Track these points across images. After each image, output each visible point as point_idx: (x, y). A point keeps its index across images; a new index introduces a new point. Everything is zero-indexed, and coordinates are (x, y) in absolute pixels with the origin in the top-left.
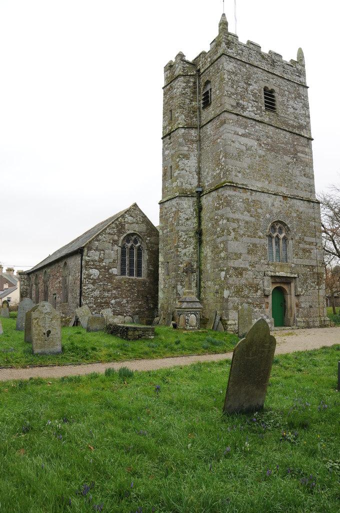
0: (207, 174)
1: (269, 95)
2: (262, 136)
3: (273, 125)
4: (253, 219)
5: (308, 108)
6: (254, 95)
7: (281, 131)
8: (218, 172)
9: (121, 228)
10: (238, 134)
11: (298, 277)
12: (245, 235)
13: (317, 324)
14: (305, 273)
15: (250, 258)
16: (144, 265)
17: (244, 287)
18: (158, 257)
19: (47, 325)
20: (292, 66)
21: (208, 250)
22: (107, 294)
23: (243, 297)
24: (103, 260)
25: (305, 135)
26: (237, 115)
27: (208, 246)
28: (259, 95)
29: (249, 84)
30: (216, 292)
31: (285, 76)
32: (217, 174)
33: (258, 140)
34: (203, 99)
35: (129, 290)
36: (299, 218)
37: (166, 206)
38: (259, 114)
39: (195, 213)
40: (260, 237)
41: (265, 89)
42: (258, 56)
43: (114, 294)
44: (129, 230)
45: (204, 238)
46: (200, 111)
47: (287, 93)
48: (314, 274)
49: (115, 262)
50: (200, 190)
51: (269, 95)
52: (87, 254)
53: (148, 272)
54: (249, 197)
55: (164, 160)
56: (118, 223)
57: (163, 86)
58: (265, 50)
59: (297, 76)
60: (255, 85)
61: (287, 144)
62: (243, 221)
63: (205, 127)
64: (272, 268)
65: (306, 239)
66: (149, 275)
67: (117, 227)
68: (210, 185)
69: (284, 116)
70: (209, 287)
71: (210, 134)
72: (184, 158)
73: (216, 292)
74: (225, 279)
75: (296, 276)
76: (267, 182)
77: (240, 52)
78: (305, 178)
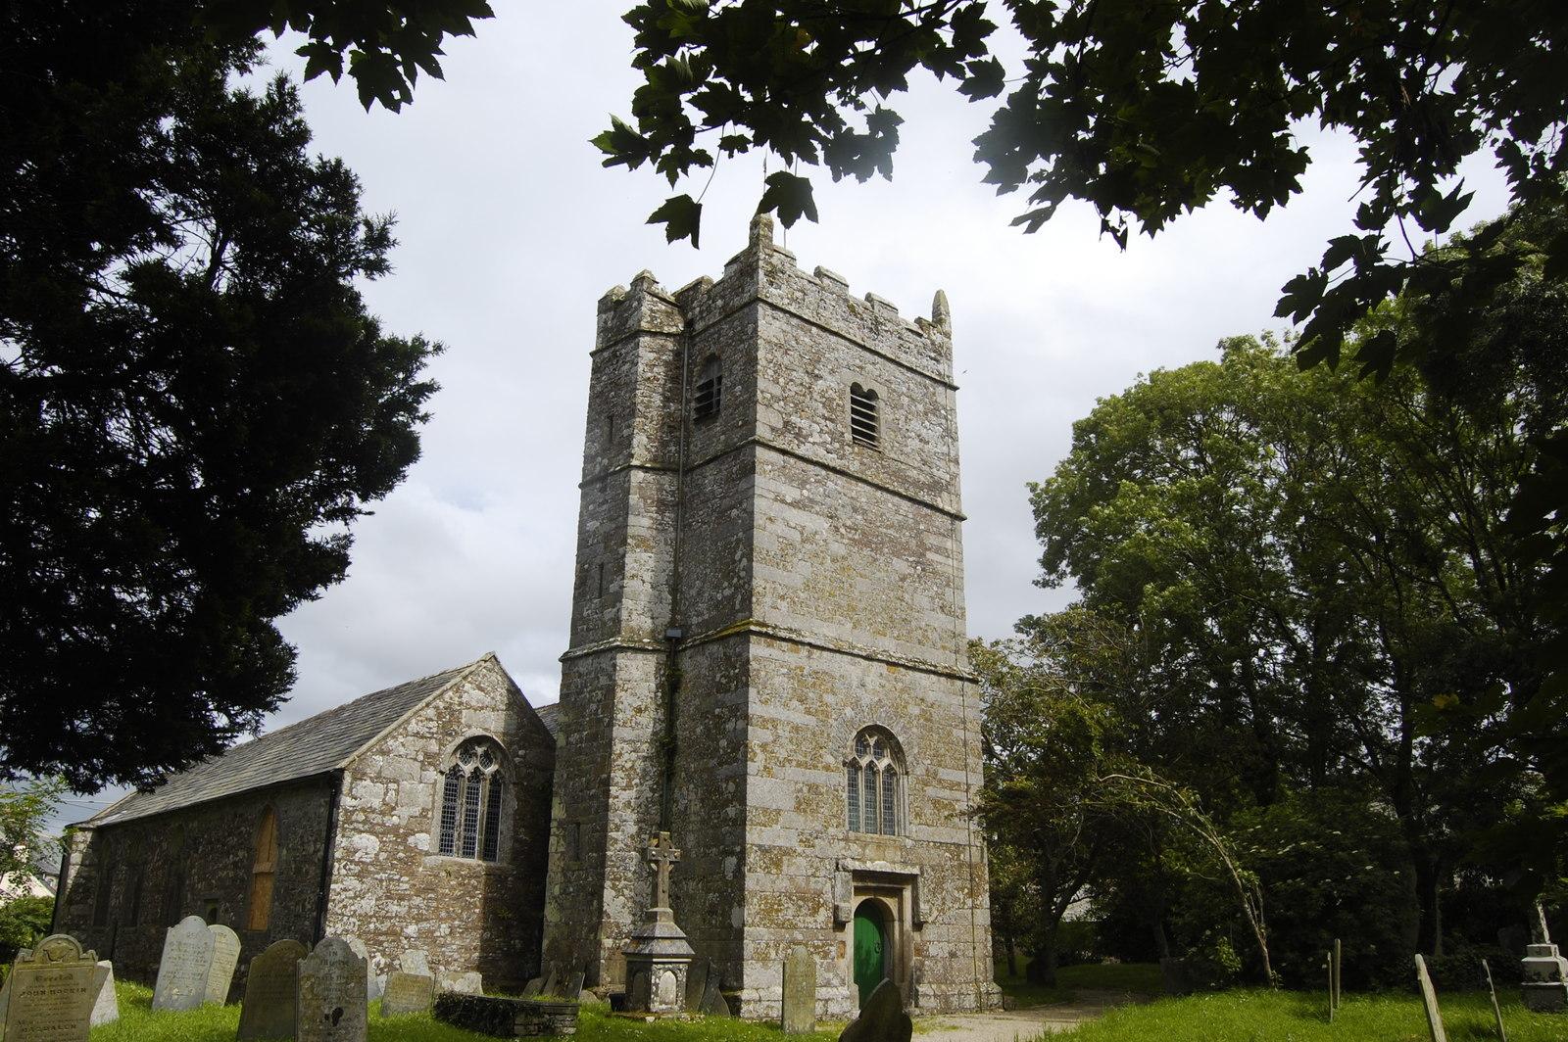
0: (698, 594)
1: (863, 401)
2: (843, 506)
3: (869, 479)
4: (811, 721)
5: (955, 440)
6: (828, 403)
7: (889, 496)
8: (727, 592)
9: (450, 721)
10: (783, 501)
11: (922, 873)
12: (790, 761)
13: (970, 1001)
14: (939, 865)
15: (800, 821)
16: (504, 826)
17: (784, 899)
18: (549, 808)
19: (334, 995)
20: (921, 336)
21: (692, 796)
22: (395, 908)
23: (781, 926)
24: (393, 809)
25: (947, 508)
26: (784, 452)
27: (692, 786)
28: (838, 405)
29: (817, 376)
30: (709, 912)
31: (904, 359)
32: (724, 597)
33: (831, 517)
34: (698, 400)
35: (457, 898)
36: (926, 720)
37: (581, 670)
38: (836, 451)
39: (659, 694)
40: (827, 768)
41: (856, 388)
42: (840, 306)
43: (418, 907)
44: (469, 727)
45: (679, 761)
46: (687, 429)
47: (905, 400)
48: (961, 866)
49: (425, 816)
50: (677, 633)
51: (863, 401)
52: (351, 790)
53: (513, 848)
54: (804, 662)
55: (583, 544)
56: (441, 705)
57: (593, 348)
58: (857, 293)
59: (932, 359)
60: (829, 378)
61: (901, 527)
62: (788, 724)
63: (698, 471)
64: (855, 848)
65: (943, 773)
66: (515, 856)
67: (440, 716)
68: (705, 624)
69: (896, 457)
70: (692, 898)
71: (713, 492)
72: (638, 546)
73: (709, 912)
74: (735, 876)
75: (916, 871)
76: (849, 625)
77: (799, 294)
78: (942, 616)
